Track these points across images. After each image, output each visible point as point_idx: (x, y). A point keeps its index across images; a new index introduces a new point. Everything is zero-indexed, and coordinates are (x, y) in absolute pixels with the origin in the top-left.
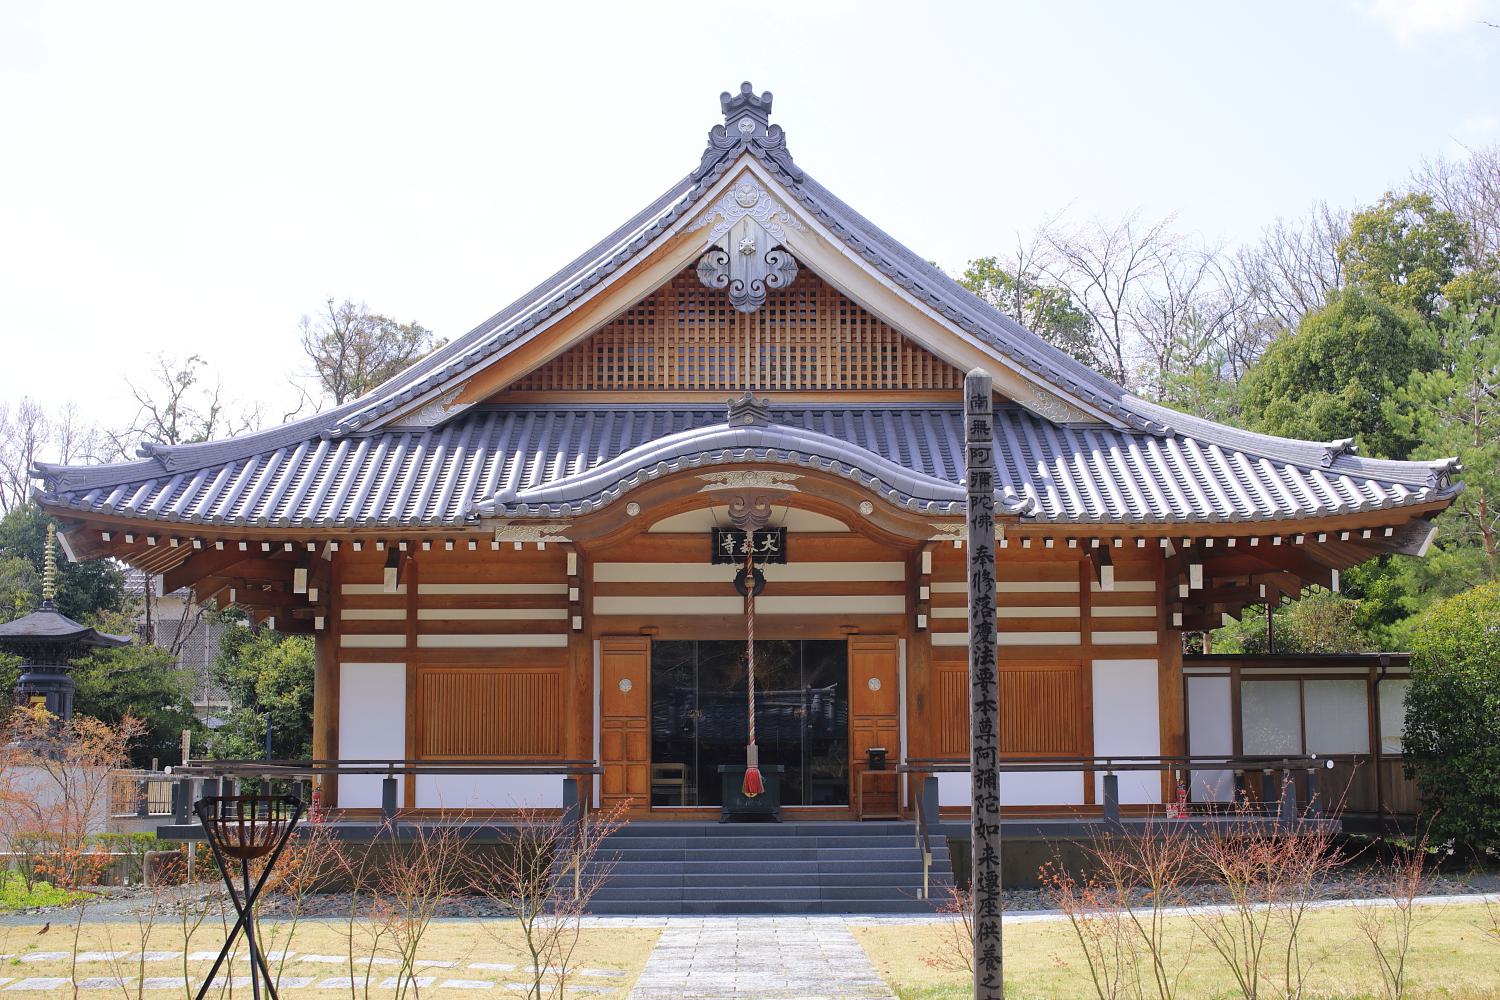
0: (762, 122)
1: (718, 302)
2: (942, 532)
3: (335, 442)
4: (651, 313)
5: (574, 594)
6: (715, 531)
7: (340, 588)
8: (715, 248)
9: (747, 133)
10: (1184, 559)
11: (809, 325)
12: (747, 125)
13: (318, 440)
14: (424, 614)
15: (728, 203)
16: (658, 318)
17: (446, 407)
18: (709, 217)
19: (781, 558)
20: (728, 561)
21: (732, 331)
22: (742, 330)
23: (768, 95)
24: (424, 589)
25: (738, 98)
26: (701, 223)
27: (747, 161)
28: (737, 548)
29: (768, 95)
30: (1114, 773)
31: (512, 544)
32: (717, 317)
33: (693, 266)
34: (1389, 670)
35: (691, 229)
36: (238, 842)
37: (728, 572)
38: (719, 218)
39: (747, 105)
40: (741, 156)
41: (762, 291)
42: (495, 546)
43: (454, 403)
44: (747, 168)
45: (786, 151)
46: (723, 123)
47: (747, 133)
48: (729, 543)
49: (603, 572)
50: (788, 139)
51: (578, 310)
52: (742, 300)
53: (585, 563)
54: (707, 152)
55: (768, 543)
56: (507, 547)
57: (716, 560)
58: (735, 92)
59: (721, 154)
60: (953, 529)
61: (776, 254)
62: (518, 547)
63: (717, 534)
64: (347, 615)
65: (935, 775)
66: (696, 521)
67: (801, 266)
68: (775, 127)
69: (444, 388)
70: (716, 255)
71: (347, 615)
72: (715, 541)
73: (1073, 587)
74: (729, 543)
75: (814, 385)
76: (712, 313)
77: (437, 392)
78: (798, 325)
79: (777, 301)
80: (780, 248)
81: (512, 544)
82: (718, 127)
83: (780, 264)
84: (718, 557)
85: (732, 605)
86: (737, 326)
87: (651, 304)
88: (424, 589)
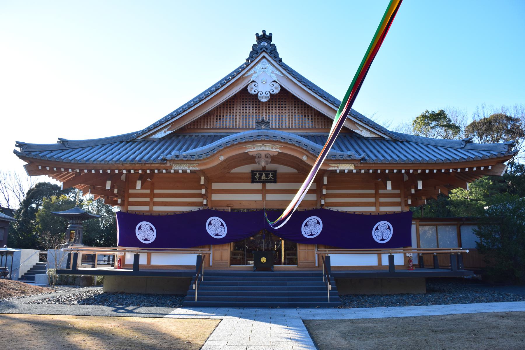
0: (269, 43)
1: (254, 99)
2: (332, 167)
3: (128, 142)
4: (233, 102)
5: (203, 191)
6: (253, 172)
7: (129, 191)
8: (253, 81)
9: (264, 46)
10: (414, 178)
11: (284, 109)
12: (264, 44)
13: (123, 142)
14: (156, 200)
15: (258, 67)
16: (235, 103)
17: (165, 132)
18: (252, 72)
19: (275, 181)
20: (257, 182)
21: (259, 110)
22: (262, 110)
23: (271, 34)
24: (156, 191)
25: (261, 35)
26: (249, 73)
27: (264, 54)
28: (260, 178)
29: (271, 34)
30: (393, 254)
31: (178, 170)
32: (254, 106)
33: (247, 87)
34: (465, 222)
35: (246, 76)
36: (420, 229)
37: (258, 186)
38: (255, 72)
39: (264, 38)
40: (262, 52)
41: (269, 95)
42: (172, 171)
43: (168, 130)
44: (264, 57)
45: (277, 52)
46: (256, 43)
47: (264, 46)
48: (257, 176)
49: (215, 186)
50: (277, 48)
51: (208, 100)
52: (263, 98)
53: (207, 180)
54: (251, 52)
55: (270, 176)
56: (176, 172)
57: (253, 182)
58: (261, 34)
59: (255, 52)
60: (336, 166)
61: (274, 83)
62: (180, 171)
63: (253, 172)
64: (131, 199)
65: (329, 255)
66: (246, 169)
67: (281, 87)
68: (273, 44)
69: (164, 125)
70: (254, 83)
71: (131, 199)
72: (252, 175)
73: (373, 191)
74: (257, 176)
75: (285, 127)
76: (253, 105)
77: (162, 126)
78: (281, 109)
79: (273, 99)
80: (275, 81)
81: (178, 170)
82: (255, 45)
83: (274, 86)
84: (254, 181)
85: (258, 197)
86: (261, 109)
87: (233, 99)
88: (156, 191)
